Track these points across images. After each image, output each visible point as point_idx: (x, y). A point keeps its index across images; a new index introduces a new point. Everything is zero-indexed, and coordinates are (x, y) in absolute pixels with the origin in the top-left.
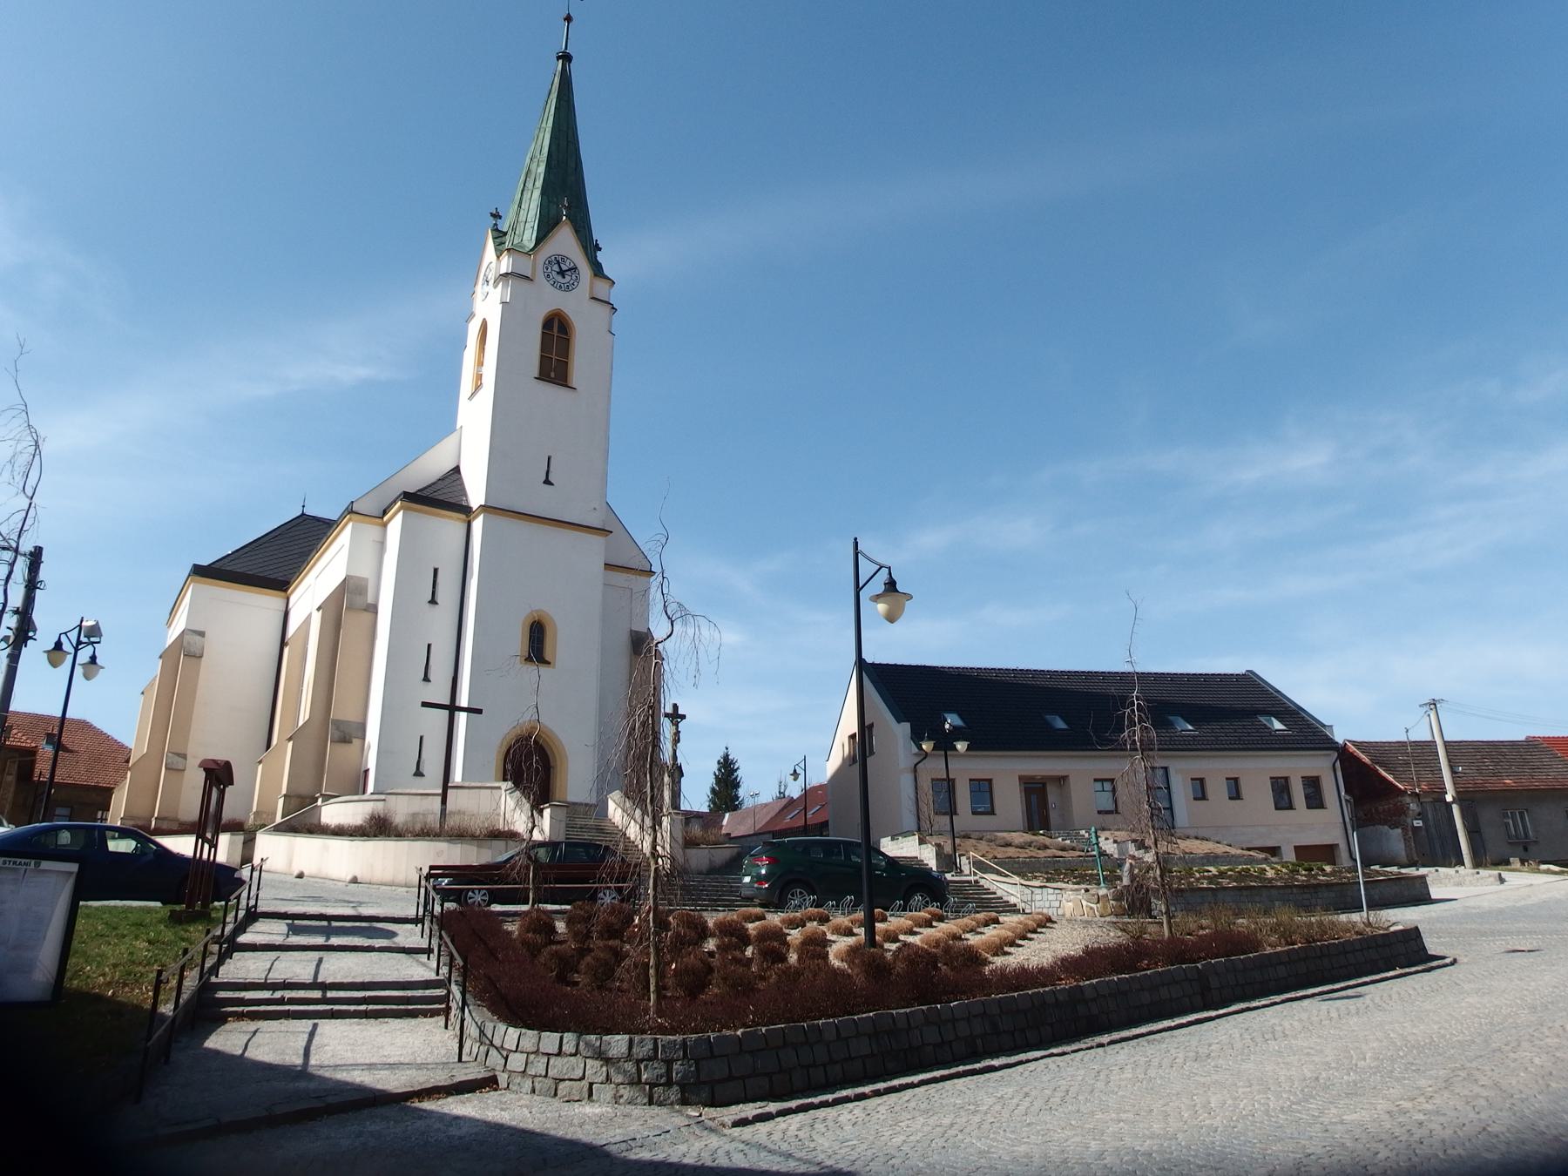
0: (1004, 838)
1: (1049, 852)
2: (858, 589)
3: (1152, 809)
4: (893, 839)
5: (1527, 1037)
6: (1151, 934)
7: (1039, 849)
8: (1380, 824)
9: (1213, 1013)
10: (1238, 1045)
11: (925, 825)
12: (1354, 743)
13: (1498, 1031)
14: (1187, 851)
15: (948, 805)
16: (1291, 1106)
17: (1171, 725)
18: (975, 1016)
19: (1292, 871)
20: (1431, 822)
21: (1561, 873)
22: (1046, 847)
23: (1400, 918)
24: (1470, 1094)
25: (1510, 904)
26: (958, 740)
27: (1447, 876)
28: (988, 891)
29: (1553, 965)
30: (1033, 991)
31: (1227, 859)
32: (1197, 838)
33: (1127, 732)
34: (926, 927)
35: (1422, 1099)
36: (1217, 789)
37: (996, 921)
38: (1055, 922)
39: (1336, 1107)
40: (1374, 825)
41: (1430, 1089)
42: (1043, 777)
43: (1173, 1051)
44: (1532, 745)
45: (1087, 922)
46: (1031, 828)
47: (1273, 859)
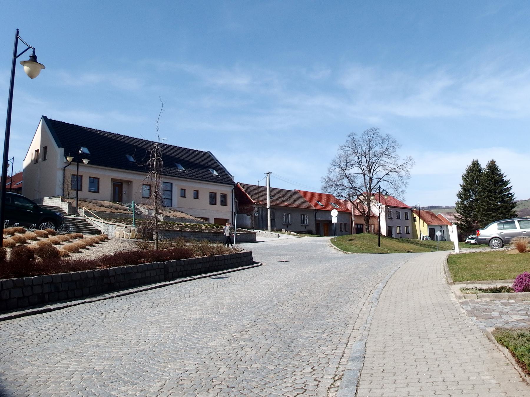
0: (101, 203)
1: (119, 211)
2: (15, 57)
3: (156, 195)
4: (49, 198)
5: (286, 299)
6: (150, 247)
7: (115, 209)
8: (244, 213)
9: (167, 283)
10: (173, 300)
11: (66, 194)
12: (240, 183)
13: (276, 296)
14: (175, 216)
15: (76, 186)
16: (186, 336)
17: (176, 167)
18: (46, 284)
19: (212, 227)
20: (260, 215)
21: (296, 235)
22: (118, 209)
23: (245, 247)
24: (264, 329)
25: (280, 244)
26: (84, 158)
27: (262, 233)
28: (89, 224)
29: (294, 268)
30: (82, 271)
31: (189, 220)
32: (179, 212)
33: (150, 160)
34: (45, 237)
35: (244, 332)
36: (190, 194)
37: (82, 237)
38: (110, 239)
39: (206, 337)
40: (242, 214)
41: (248, 326)
42: (122, 180)
43: (143, 302)
44: (295, 193)
45: (124, 240)
46: (114, 200)
47: (206, 222)
